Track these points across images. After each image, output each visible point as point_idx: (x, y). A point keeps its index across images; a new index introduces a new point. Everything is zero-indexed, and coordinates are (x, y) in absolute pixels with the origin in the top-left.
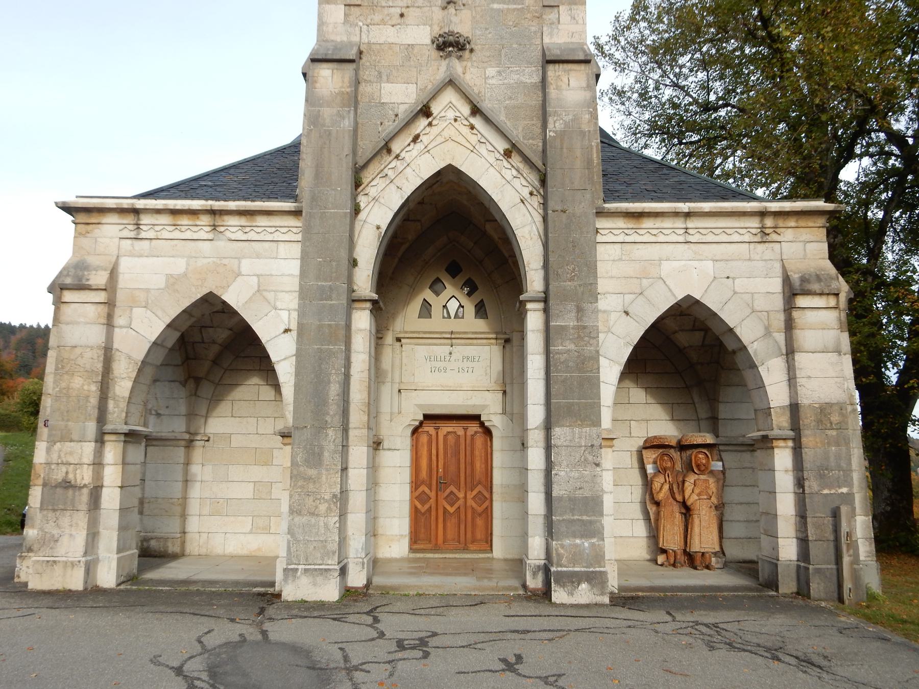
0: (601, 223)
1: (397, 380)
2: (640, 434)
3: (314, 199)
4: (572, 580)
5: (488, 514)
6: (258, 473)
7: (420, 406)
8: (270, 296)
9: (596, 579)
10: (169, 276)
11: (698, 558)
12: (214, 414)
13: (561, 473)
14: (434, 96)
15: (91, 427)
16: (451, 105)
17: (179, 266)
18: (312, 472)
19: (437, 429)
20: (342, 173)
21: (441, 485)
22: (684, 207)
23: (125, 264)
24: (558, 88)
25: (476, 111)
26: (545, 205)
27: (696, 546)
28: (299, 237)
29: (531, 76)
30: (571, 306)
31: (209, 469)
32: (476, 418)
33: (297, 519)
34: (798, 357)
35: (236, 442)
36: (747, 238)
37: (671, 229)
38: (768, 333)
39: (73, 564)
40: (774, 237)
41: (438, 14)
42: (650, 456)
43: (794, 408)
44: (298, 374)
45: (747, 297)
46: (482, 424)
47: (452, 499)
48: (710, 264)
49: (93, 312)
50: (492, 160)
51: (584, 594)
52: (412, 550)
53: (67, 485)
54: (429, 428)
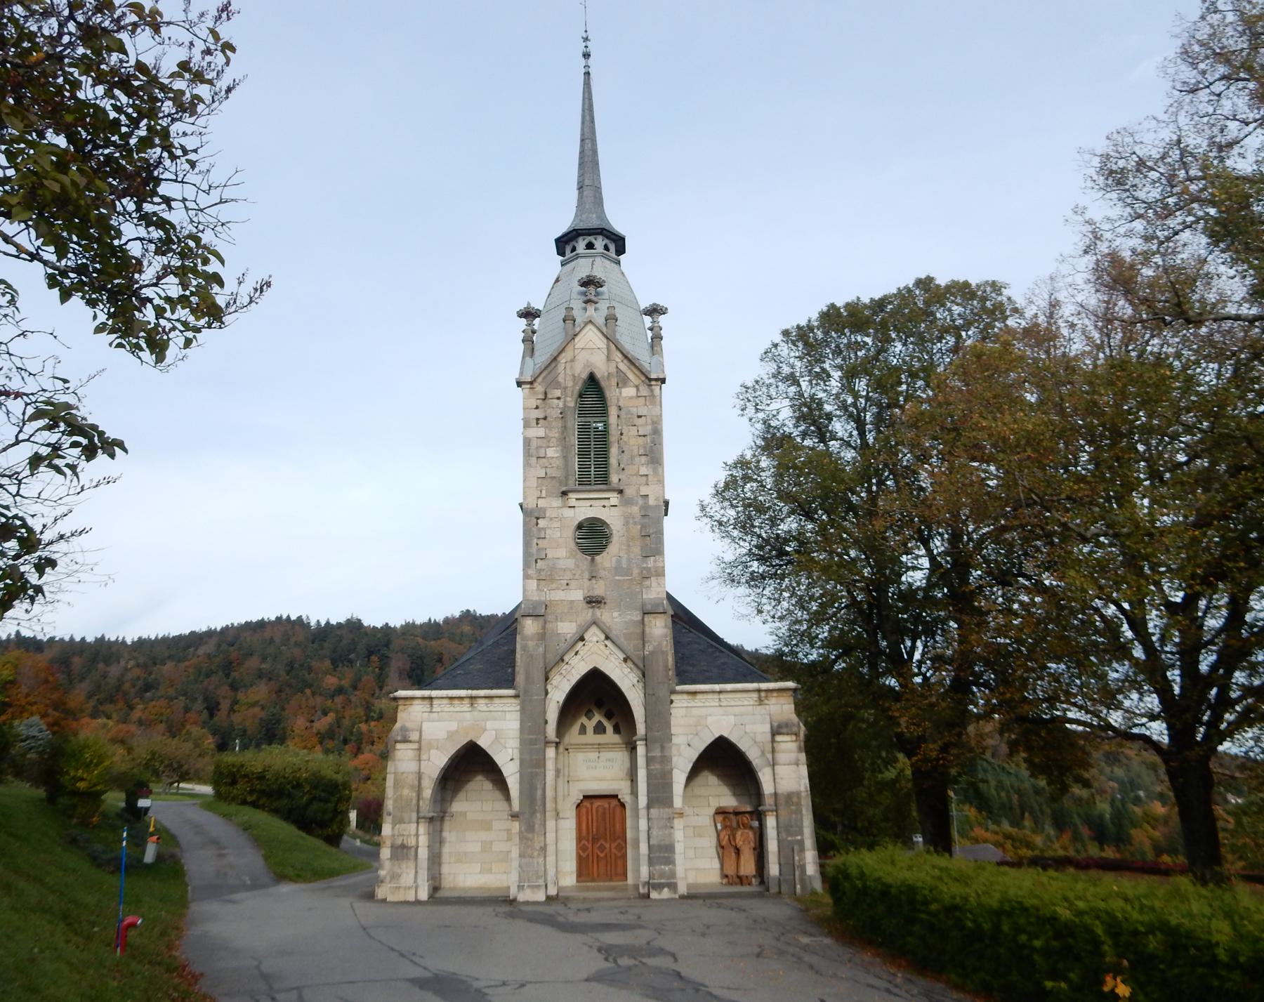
0: (674, 697)
1: (566, 773)
2: (716, 803)
3: (526, 692)
4: (659, 887)
5: (624, 857)
6: (483, 835)
7: (581, 791)
8: (502, 741)
9: (673, 887)
10: (448, 732)
11: (744, 879)
12: (457, 799)
13: (654, 832)
14: (586, 630)
15: (414, 816)
16: (594, 634)
17: (453, 726)
18: (530, 836)
19: (592, 804)
20: (539, 676)
21: (595, 840)
22: (717, 687)
23: (426, 726)
24: (650, 627)
25: (607, 638)
26: (645, 688)
27: (742, 873)
28: (518, 708)
29: (636, 616)
30: (658, 745)
31: (453, 834)
32: (616, 797)
33: (523, 860)
34: (776, 767)
35: (470, 816)
36: (752, 703)
37: (712, 700)
38: (763, 753)
39: (409, 888)
40: (766, 702)
41: (587, 583)
42: (720, 818)
43: (776, 794)
44: (521, 784)
45: (752, 735)
46: (619, 800)
47: (602, 848)
48: (733, 717)
49: (411, 754)
50: (617, 663)
51: (666, 894)
52: (578, 881)
53: (403, 846)
54: (587, 804)
